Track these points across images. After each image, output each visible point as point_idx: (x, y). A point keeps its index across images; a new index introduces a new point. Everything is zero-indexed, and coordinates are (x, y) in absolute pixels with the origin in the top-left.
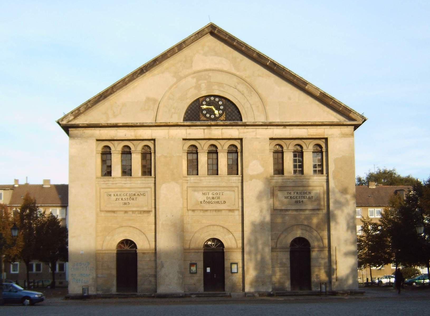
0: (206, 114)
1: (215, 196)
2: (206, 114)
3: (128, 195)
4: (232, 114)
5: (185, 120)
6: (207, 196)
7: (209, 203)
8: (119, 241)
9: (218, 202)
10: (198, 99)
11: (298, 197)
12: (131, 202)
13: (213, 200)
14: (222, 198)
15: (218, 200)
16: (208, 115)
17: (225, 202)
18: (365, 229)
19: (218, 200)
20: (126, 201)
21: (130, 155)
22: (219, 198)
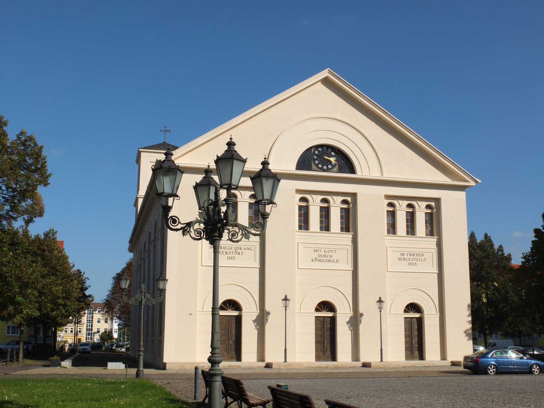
0: (318, 164)
1: (327, 254)
2: (318, 164)
3: (233, 248)
4: (346, 164)
5: (299, 167)
6: (319, 253)
7: (320, 261)
8: (425, 318)
9: (330, 261)
10: (311, 148)
11: (411, 260)
12: (237, 256)
13: (325, 258)
14: (335, 257)
15: (330, 259)
16: (320, 166)
17: (337, 261)
18: (119, 311)
19: (330, 259)
20: (231, 255)
21: (243, 163)
22: (331, 256)
